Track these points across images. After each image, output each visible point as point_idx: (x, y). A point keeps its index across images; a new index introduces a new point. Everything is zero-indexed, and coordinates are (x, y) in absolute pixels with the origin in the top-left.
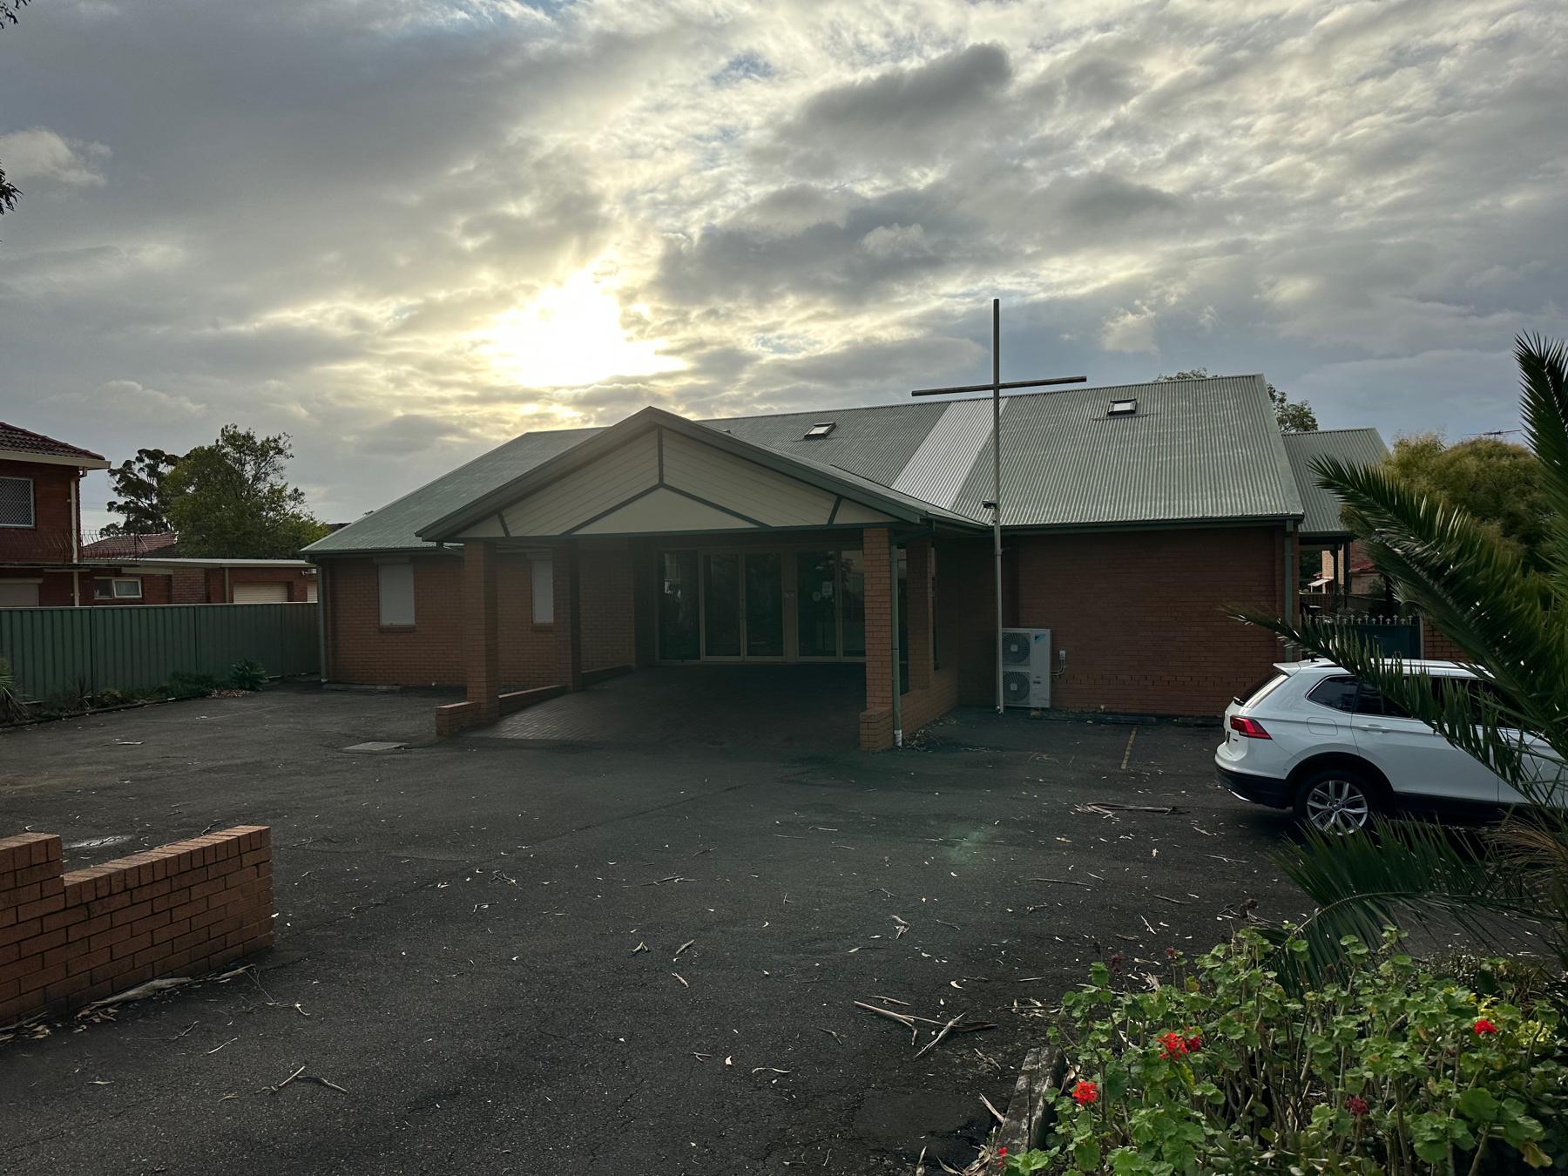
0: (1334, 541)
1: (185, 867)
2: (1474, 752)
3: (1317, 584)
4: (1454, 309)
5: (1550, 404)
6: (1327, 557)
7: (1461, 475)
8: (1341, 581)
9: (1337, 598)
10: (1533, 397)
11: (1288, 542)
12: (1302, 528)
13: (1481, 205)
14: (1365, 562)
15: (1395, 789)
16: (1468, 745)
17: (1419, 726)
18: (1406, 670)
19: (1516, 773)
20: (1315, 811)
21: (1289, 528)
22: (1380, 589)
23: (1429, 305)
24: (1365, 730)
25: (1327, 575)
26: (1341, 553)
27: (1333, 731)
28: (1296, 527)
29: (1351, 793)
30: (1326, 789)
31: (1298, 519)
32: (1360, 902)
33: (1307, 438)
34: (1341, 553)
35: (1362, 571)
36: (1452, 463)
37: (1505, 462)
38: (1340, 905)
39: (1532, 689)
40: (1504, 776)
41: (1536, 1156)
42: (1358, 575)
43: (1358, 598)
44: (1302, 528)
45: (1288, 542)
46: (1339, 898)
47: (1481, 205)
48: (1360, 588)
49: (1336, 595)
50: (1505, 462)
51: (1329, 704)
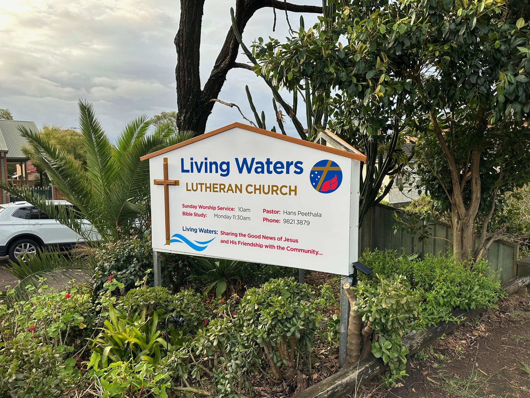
0: (21, 161)
1: (225, 49)
2: (67, 225)
3: (15, 176)
4: (53, 83)
5: (87, 120)
6: (18, 166)
7: (65, 142)
8: (24, 176)
9: (22, 182)
10: (82, 118)
11: (2, 160)
12: (8, 156)
13: (65, 50)
14: (32, 169)
15: (45, 243)
16: (66, 223)
17: (53, 221)
18: (47, 204)
19: (79, 229)
20: (17, 255)
21: (3, 155)
22: (38, 178)
23: (44, 80)
24: (34, 225)
25: (19, 173)
26: (23, 165)
27: (22, 226)
28: (5, 155)
29: (30, 247)
30: (21, 247)
31: (6, 152)
32: (34, 276)
33: (8, 122)
34: (23, 165)
35: (32, 172)
36: (63, 137)
37: (76, 138)
38: (28, 279)
39: (83, 204)
40: (76, 231)
41: (82, 326)
42: (30, 173)
43: (30, 181)
44: (8, 156)
45: (2, 160)
46: (27, 276)
47: (65, 50)
48: (31, 178)
49: (22, 180)
50: (76, 138)
51: (20, 217)
